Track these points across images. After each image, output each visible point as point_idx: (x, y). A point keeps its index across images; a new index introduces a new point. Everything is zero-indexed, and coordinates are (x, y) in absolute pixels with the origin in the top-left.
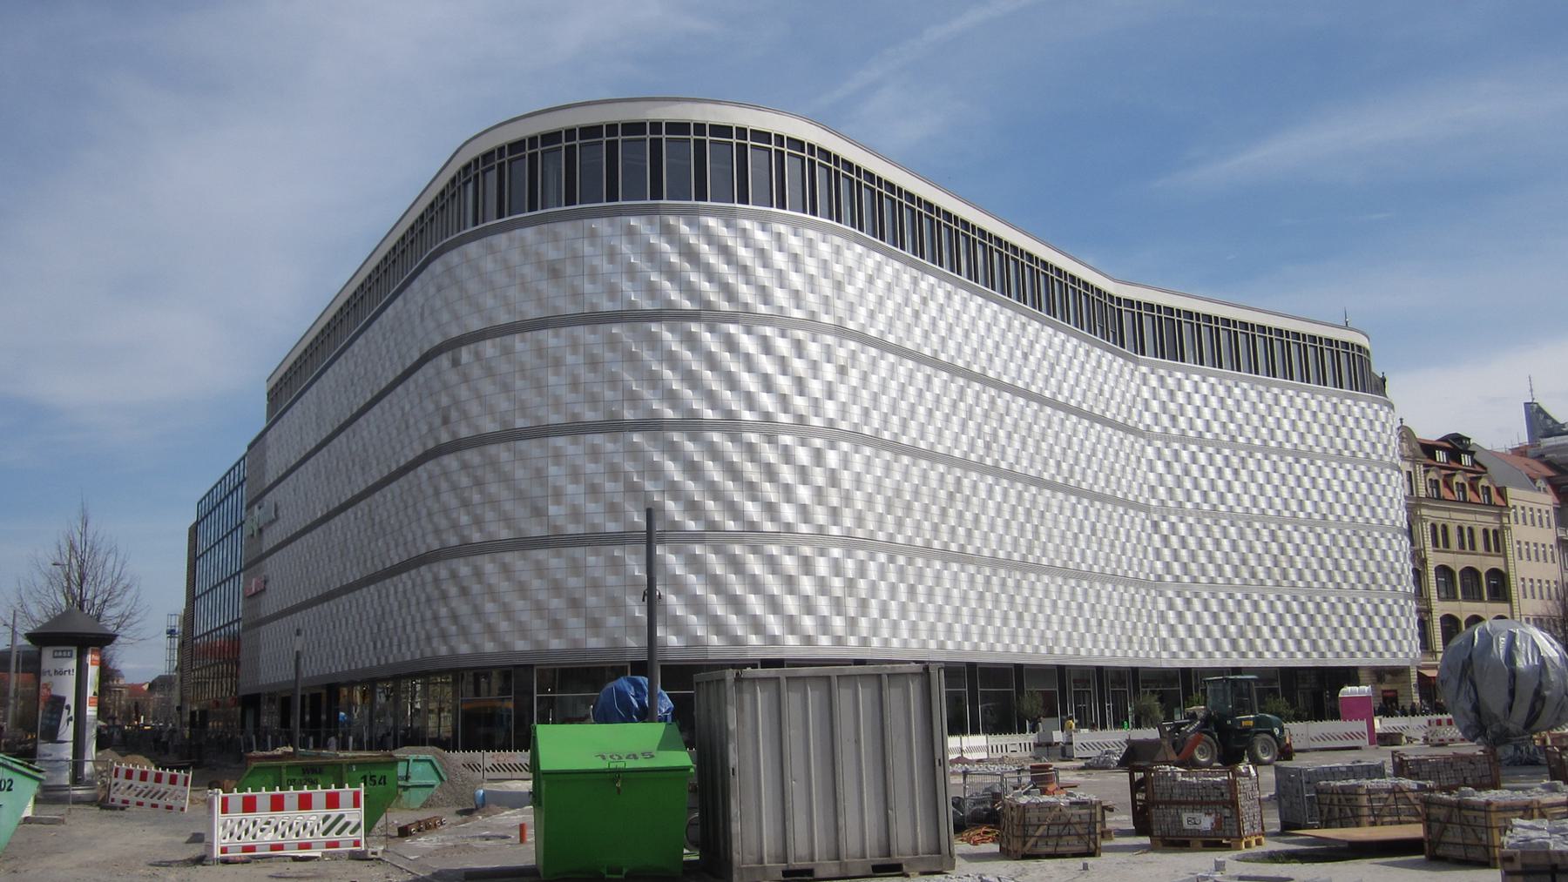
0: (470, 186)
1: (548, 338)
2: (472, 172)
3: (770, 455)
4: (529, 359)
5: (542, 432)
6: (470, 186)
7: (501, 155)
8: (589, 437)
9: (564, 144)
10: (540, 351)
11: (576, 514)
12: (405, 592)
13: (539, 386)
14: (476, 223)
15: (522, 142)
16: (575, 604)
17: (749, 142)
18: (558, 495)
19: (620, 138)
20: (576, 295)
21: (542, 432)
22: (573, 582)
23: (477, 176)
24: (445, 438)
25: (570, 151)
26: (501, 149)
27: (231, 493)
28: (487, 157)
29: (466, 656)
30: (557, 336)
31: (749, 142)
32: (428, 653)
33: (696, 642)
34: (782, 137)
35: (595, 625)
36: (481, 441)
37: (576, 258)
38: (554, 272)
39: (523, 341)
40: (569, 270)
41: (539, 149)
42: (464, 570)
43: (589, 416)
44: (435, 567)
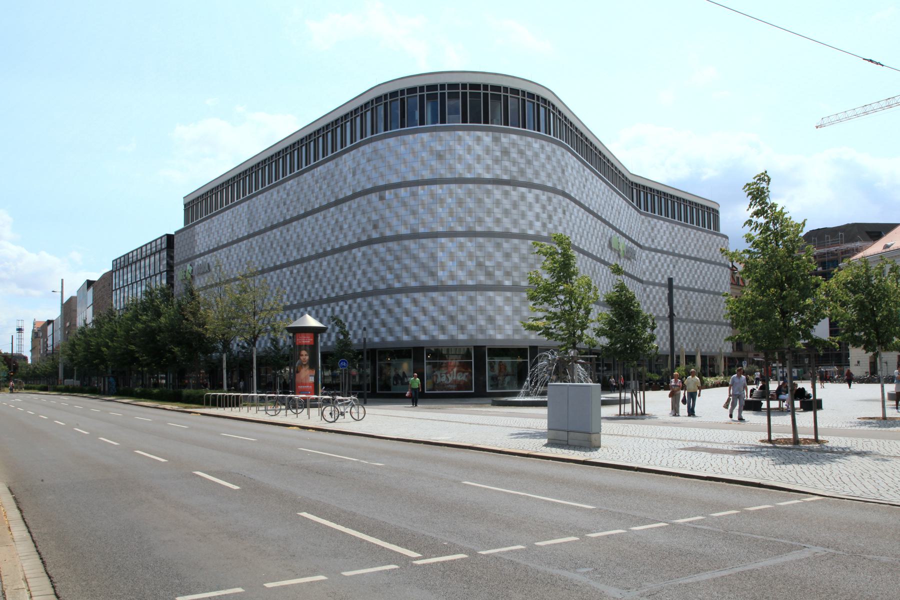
1: (438, 189)
4: (426, 199)
5: (434, 235)
7: (386, 99)
10: (432, 195)
11: (452, 276)
13: (432, 213)
15: (381, 97)
18: (443, 266)
19: (389, 100)
20: (451, 168)
21: (434, 235)
22: (451, 308)
33: (415, 338)
35: (462, 328)
36: (398, 238)
37: (451, 150)
38: (440, 157)
40: (448, 156)
41: (406, 96)
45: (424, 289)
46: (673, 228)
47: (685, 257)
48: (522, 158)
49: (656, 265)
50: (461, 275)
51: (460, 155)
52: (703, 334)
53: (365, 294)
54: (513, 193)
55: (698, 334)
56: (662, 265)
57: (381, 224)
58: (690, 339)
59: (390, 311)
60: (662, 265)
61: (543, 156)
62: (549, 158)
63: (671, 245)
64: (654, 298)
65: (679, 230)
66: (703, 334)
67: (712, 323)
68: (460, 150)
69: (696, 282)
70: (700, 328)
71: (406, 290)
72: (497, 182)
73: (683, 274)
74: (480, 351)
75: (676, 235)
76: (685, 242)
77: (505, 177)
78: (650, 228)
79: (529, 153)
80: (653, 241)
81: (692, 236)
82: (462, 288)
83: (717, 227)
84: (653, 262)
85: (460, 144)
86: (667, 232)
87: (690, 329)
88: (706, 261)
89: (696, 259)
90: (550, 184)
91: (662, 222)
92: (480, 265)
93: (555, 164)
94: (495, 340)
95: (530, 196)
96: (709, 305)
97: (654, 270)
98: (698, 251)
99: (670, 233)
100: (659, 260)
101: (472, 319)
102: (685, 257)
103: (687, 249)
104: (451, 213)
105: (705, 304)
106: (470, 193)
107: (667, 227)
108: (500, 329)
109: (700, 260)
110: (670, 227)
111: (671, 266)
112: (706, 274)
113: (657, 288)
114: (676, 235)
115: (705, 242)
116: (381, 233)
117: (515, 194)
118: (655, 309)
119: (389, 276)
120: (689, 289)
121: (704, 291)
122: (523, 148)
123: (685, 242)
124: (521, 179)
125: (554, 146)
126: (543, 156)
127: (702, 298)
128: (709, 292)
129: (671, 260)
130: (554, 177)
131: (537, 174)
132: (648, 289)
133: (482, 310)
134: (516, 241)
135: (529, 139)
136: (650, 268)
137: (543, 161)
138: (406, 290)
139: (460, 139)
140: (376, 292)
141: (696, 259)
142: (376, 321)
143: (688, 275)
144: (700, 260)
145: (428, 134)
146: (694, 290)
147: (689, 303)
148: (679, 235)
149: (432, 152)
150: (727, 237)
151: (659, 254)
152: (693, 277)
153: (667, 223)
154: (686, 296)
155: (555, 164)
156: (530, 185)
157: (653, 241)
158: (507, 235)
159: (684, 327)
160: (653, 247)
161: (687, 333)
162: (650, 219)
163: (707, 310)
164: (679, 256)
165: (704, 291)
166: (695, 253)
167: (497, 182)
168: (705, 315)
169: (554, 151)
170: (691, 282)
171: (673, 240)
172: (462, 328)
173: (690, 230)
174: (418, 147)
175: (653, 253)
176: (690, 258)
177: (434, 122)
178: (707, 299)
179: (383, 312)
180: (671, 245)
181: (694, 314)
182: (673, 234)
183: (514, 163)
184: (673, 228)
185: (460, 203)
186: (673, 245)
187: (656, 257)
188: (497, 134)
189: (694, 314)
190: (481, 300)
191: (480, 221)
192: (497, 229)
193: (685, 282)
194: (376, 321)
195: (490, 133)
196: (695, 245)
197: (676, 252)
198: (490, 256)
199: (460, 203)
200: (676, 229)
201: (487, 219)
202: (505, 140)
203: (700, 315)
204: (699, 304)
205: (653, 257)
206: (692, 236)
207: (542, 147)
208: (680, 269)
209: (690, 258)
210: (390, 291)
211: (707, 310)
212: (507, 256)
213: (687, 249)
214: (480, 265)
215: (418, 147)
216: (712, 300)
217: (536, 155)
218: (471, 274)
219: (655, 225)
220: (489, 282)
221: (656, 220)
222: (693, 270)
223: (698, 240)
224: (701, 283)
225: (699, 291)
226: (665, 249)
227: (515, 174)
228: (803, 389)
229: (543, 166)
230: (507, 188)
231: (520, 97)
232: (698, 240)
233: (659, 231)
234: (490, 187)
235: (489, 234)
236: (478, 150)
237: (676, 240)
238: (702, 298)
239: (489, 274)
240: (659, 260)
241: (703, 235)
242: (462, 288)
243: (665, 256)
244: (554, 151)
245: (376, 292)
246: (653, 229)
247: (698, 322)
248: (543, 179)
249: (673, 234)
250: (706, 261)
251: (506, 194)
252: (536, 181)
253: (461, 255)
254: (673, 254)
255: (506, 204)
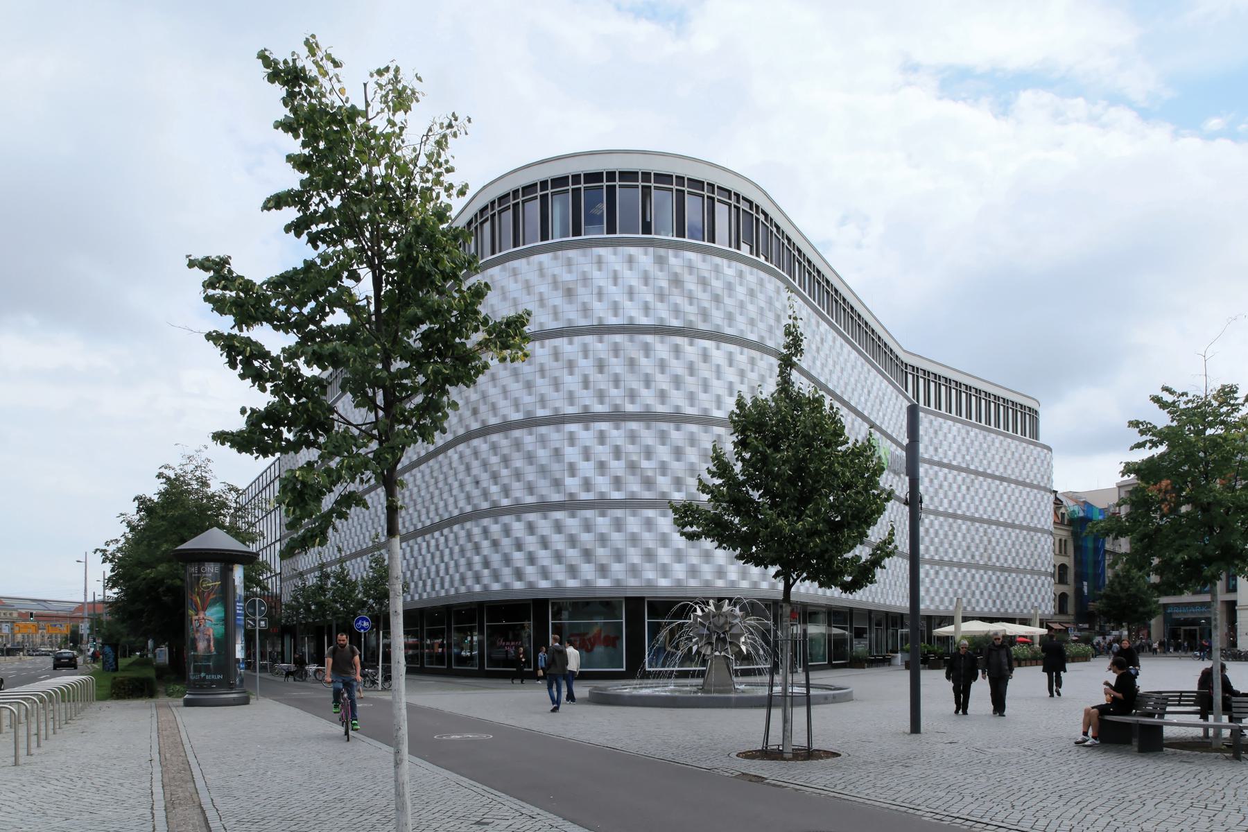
0: (487, 226)
2: (473, 226)
3: (1101, 810)
5: (558, 420)
6: (487, 226)
8: (597, 424)
9: (605, 184)
12: (437, 546)
14: (493, 253)
16: (587, 555)
17: (653, 184)
23: (493, 216)
24: (475, 426)
25: (576, 192)
26: (516, 192)
27: (264, 489)
28: (503, 199)
29: (497, 592)
30: (571, 343)
31: (617, 183)
32: (463, 590)
34: (713, 186)
36: (506, 427)
39: (542, 346)
40: (581, 290)
42: (495, 529)
43: (598, 408)
44: (468, 525)
45: (544, 507)
46: (968, 433)
47: (985, 475)
48: (705, 291)
49: (941, 486)
50: (602, 484)
51: (600, 288)
52: (1010, 587)
53: (462, 518)
54: (688, 349)
55: (1002, 587)
56: (950, 486)
57: (483, 408)
58: (990, 595)
59: (495, 544)
60: (950, 486)
61: (741, 291)
62: (752, 293)
63: (963, 457)
64: (937, 533)
65: (976, 435)
66: (1010, 587)
67: (1025, 571)
68: (600, 278)
69: (1002, 512)
70: (1006, 579)
71: (518, 510)
72: (661, 330)
73: (981, 500)
74: (635, 604)
75: (972, 442)
76: (985, 454)
77: (676, 323)
78: (931, 431)
79: (717, 284)
80: (936, 450)
81: (997, 444)
82: (603, 504)
83: (1035, 434)
84: (936, 482)
85: (600, 269)
86: (959, 439)
87: (990, 580)
88: (1017, 482)
89: (1002, 479)
90: (753, 337)
91: (950, 423)
92: (632, 467)
93: (763, 304)
94: (656, 588)
95: (718, 353)
96: (1021, 545)
97: (936, 492)
98: (1005, 468)
99: (963, 440)
100: (945, 479)
101: (619, 556)
102: (985, 475)
103: (989, 463)
104: (586, 383)
105: (1013, 544)
106: (616, 350)
107: (959, 431)
108: (664, 571)
109: (1009, 481)
110: (963, 431)
111: (964, 488)
112: (1017, 501)
113: (941, 519)
114: (972, 442)
115: (1017, 455)
116: (483, 421)
117: (691, 349)
118: (937, 550)
119: (494, 489)
120: (989, 522)
121: (1013, 526)
122: (706, 274)
123: (985, 454)
124: (702, 326)
125: (762, 274)
126: (741, 291)
127: (1009, 535)
128: (1021, 527)
129: (964, 480)
130: (762, 326)
131: (730, 317)
132: (969, 557)
133: (634, 540)
134: (693, 428)
135: (717, 260)
136: (931, 490)
137: (742, 297)
138: (518, 510)
139: (600, 261)
140: (476, 515)
141: (1002, 479)
142: (477, 559)
143: (989, 502)
144: (1009, 481)
145: (551, 254)
146: (998, 523)
147: (990, 542)
148: (976, 443)
149: (555, 283)
150: (1049, 449)
151: (946, 470)
152: (997, 504)
153: (959, 425)
154: (985, 532)
155: (763, 304)
156: (717, 336)
157: (936, 450)
158: (678, 418)
159: (982, 577)
160: (936, 459)
161: (986, 587)
162: (932, 417)
163: (1017, 553)
164: (977, 473)
165: (1013, 526)
166: (1001, 469)
167: (661, 330)
168: (1014, 561)
169: (761, 282)
170: (993, 511)
171: (968, 450)
172: (603, 570)
173: (993, 435)
174: (533, 277)
175: (936, 468)
176: (993, 477)
177: (565, 234)
178: (1017, 537)
179: (485, 544)
180: (963, 457)
181: (998, 558)
182: (968, 441)
183: (691, 298)
184: (968, 433)
185: (601, 366)
186: (968, 458)
187: (941, 474)
188: (662, 251)
189: (998, 558)
190: (633, 523)
191: (632, 396)
192: (660, 409)
193: (985, 511)
194: (477, 559)
195: (651, 249)
196: (1001, 459)
197: (972, 467)
198: (648, 453)
199: (601, 366)
200: (972, 434)
201: (644, 392)
202: (675, 260)
203: (1006, 560)
204: (1006, 544)
205: (936, 474)
206: (997, 444)
207: (741, 274)
208: (977, 492)
209: (993, 477)
210: (496, 512)
211: (1017, 553)
212: (678, 453)
213: (989, 463)
214: (632, 467)
215: (533, 277)
216: (1025, 539)
217: (730, 287)
218: (617, 482)
219: (941, 427)
220: (647, 495)
221: (941, 420)
222: (997, 495)
223: (1005, 452)
224: (1009, 513)
225: (1006, 525)
226: (954, 463)
227: (693, 318)
228: (265, 456)
229: (742, 305)
230: (679, 340)
231: (706, 193)
232: (1005, 452)
233: (945, 436)
234: (649, 338)
235: (647, 417)
236: (631, 278)
237: (972, 451)
238: (1009, 535)
239: (648, 483)
240: (945, 479)
241: (1014, 444)
242: (603, 504)
243: (955, 472)
244: (761, 282)
245: (476, 515)
246: (936, 432)
247: (1002, 569)
248: (739, 327)
249: (968, 441)
250: (1017, 482)
251: (677, 350)
252: (728, 331)
253: (602, 452)
254: (967, 470)
255: (677, 367)
